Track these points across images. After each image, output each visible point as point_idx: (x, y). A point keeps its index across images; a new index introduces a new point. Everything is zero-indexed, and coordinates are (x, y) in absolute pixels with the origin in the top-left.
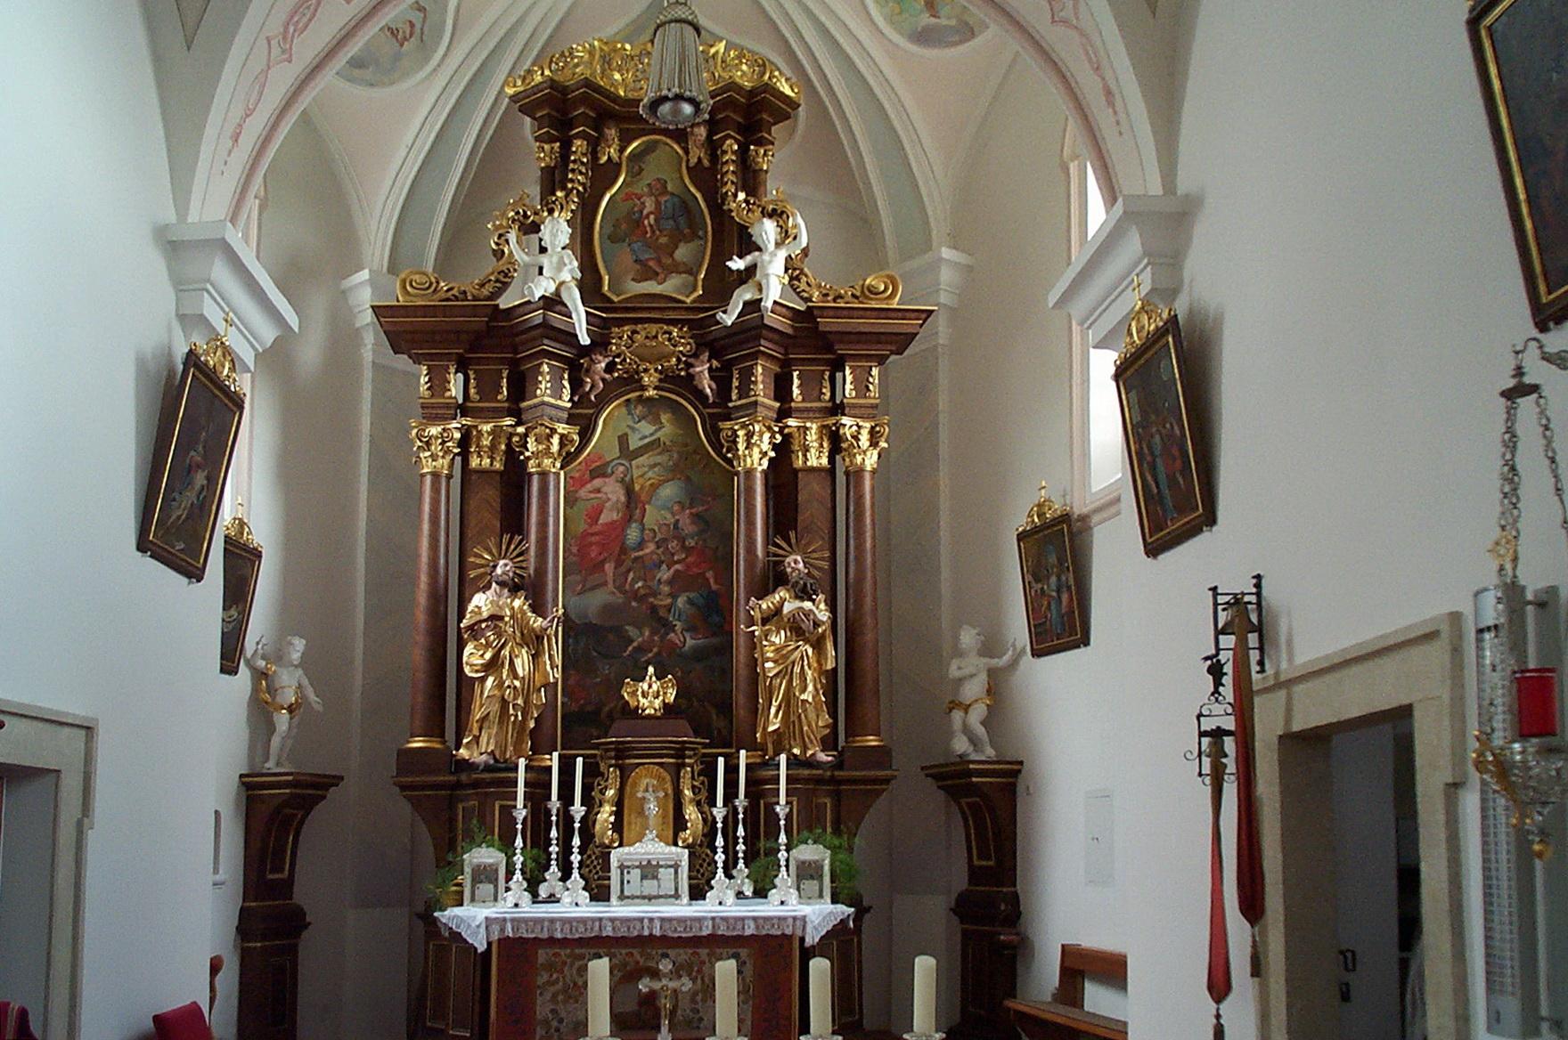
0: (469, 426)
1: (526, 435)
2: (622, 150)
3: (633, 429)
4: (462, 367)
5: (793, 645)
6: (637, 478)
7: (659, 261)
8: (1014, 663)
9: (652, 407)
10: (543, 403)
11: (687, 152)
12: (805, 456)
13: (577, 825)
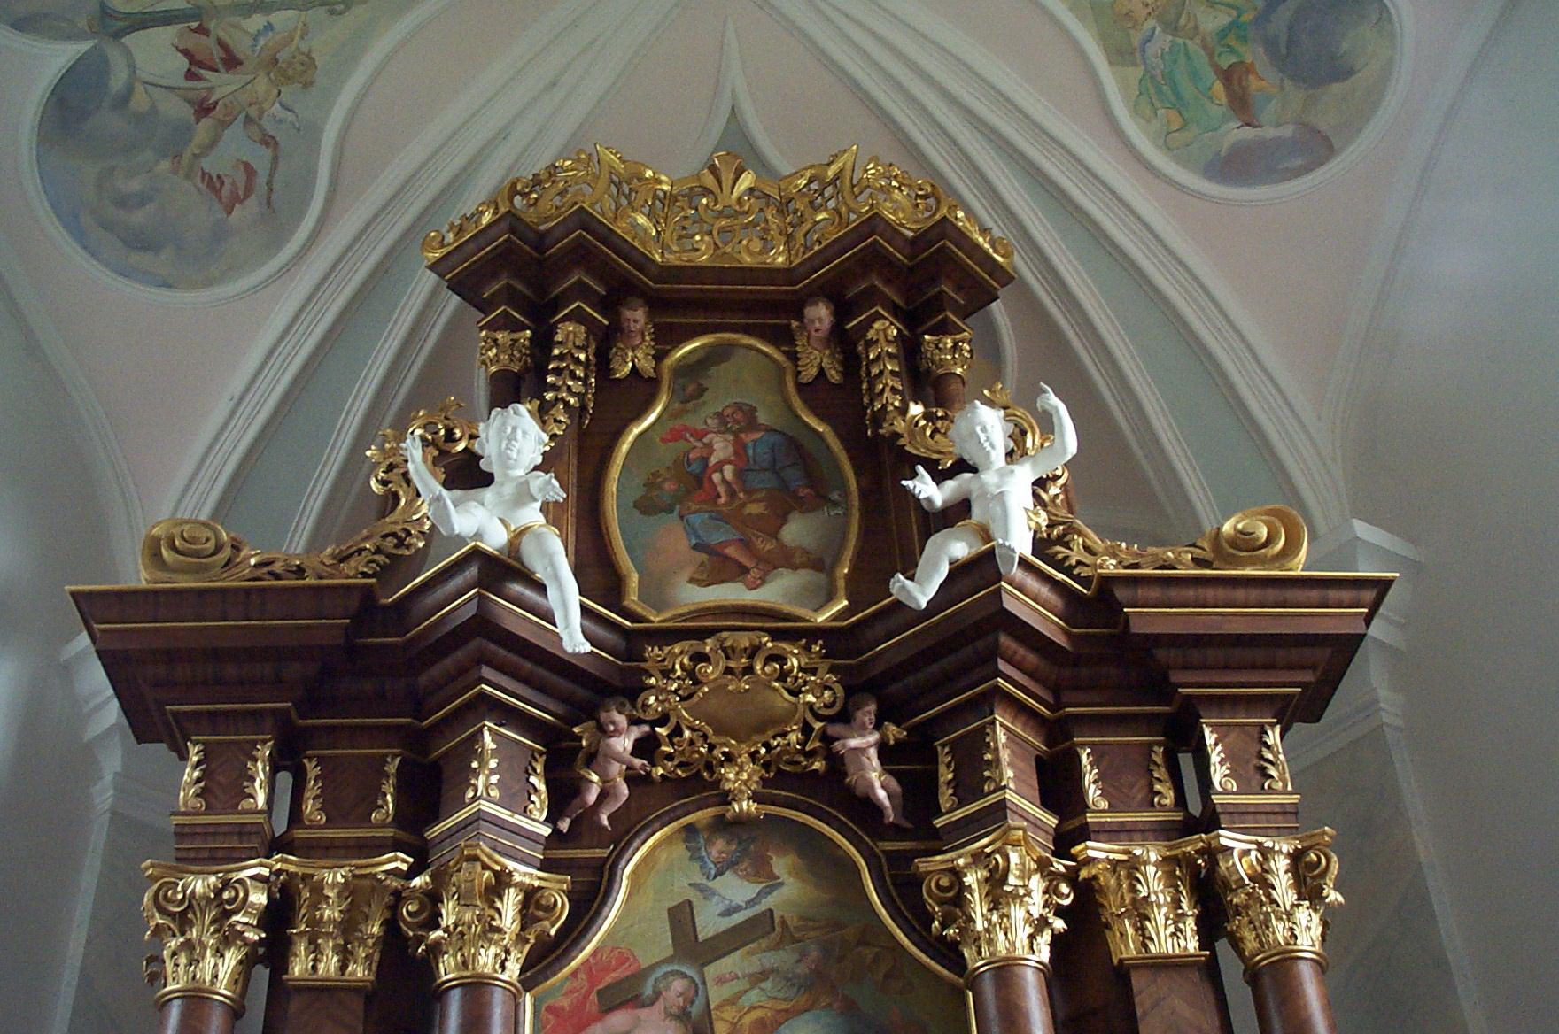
0: (291, 875)
2: (659, 357)
3: (702, 889)
4: (287, 759)
6: (719, 1007)
7: (746, 544)
11: (793, 357)
12: (1141, 930)
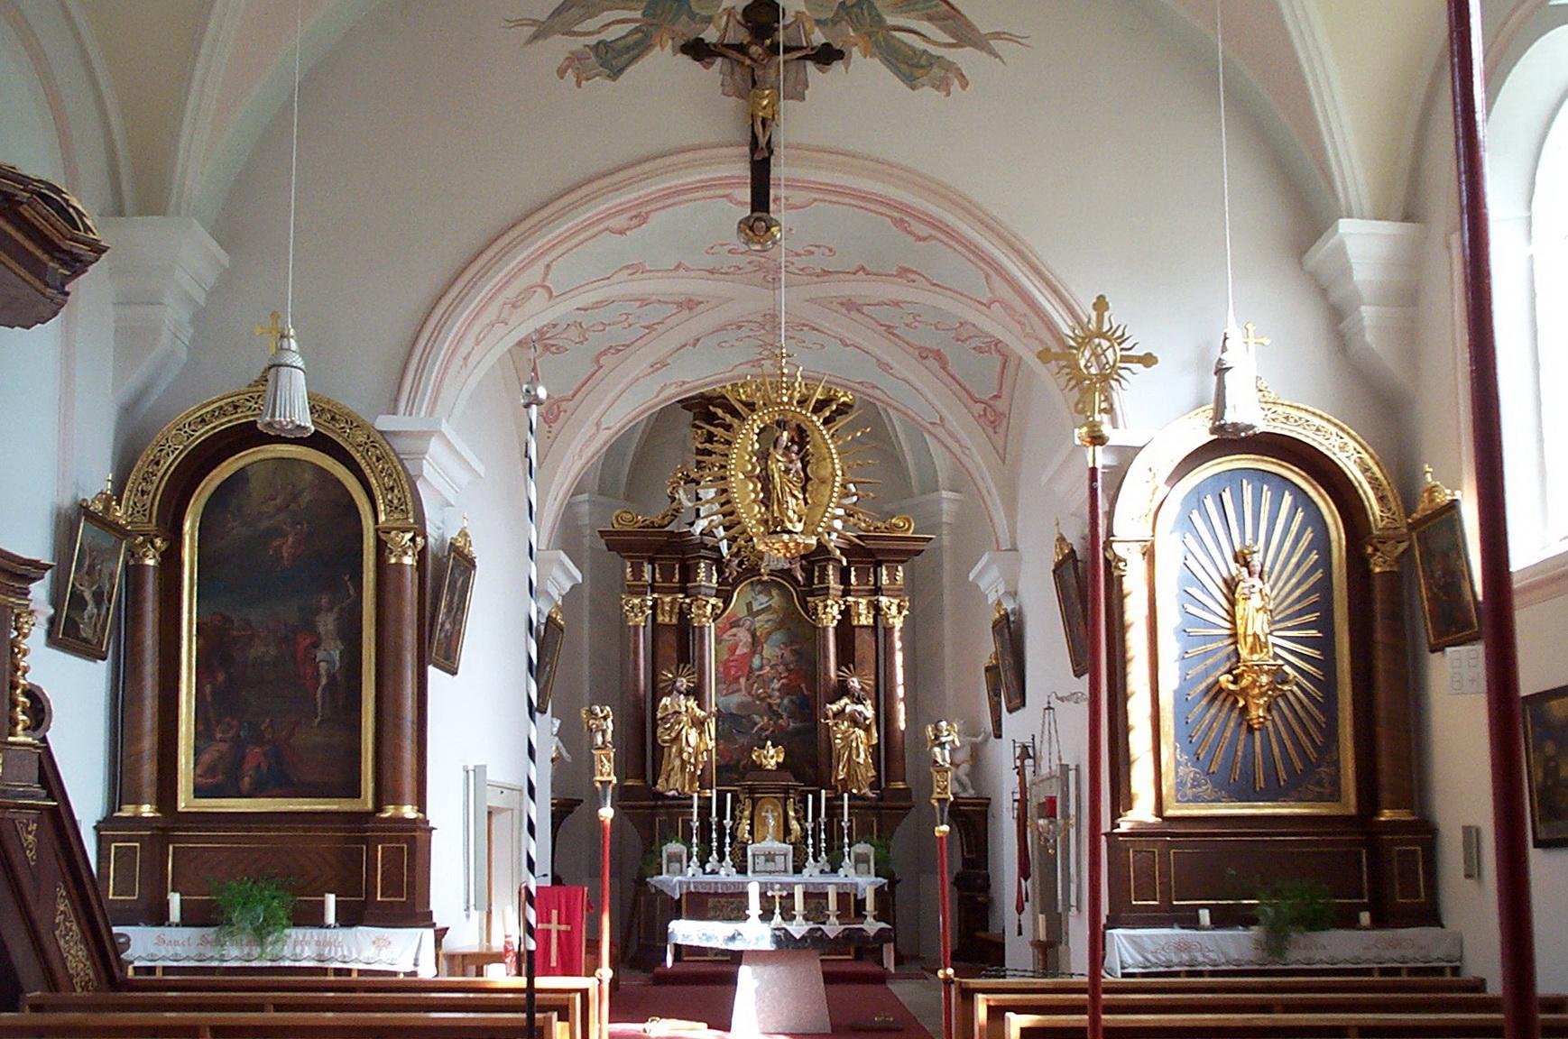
1: (692, 603)
4: (651, 562)
5: (851, 730)
8: (986, 740)
9: (766, 587)
10: (700, 586)
13: (728, 831)
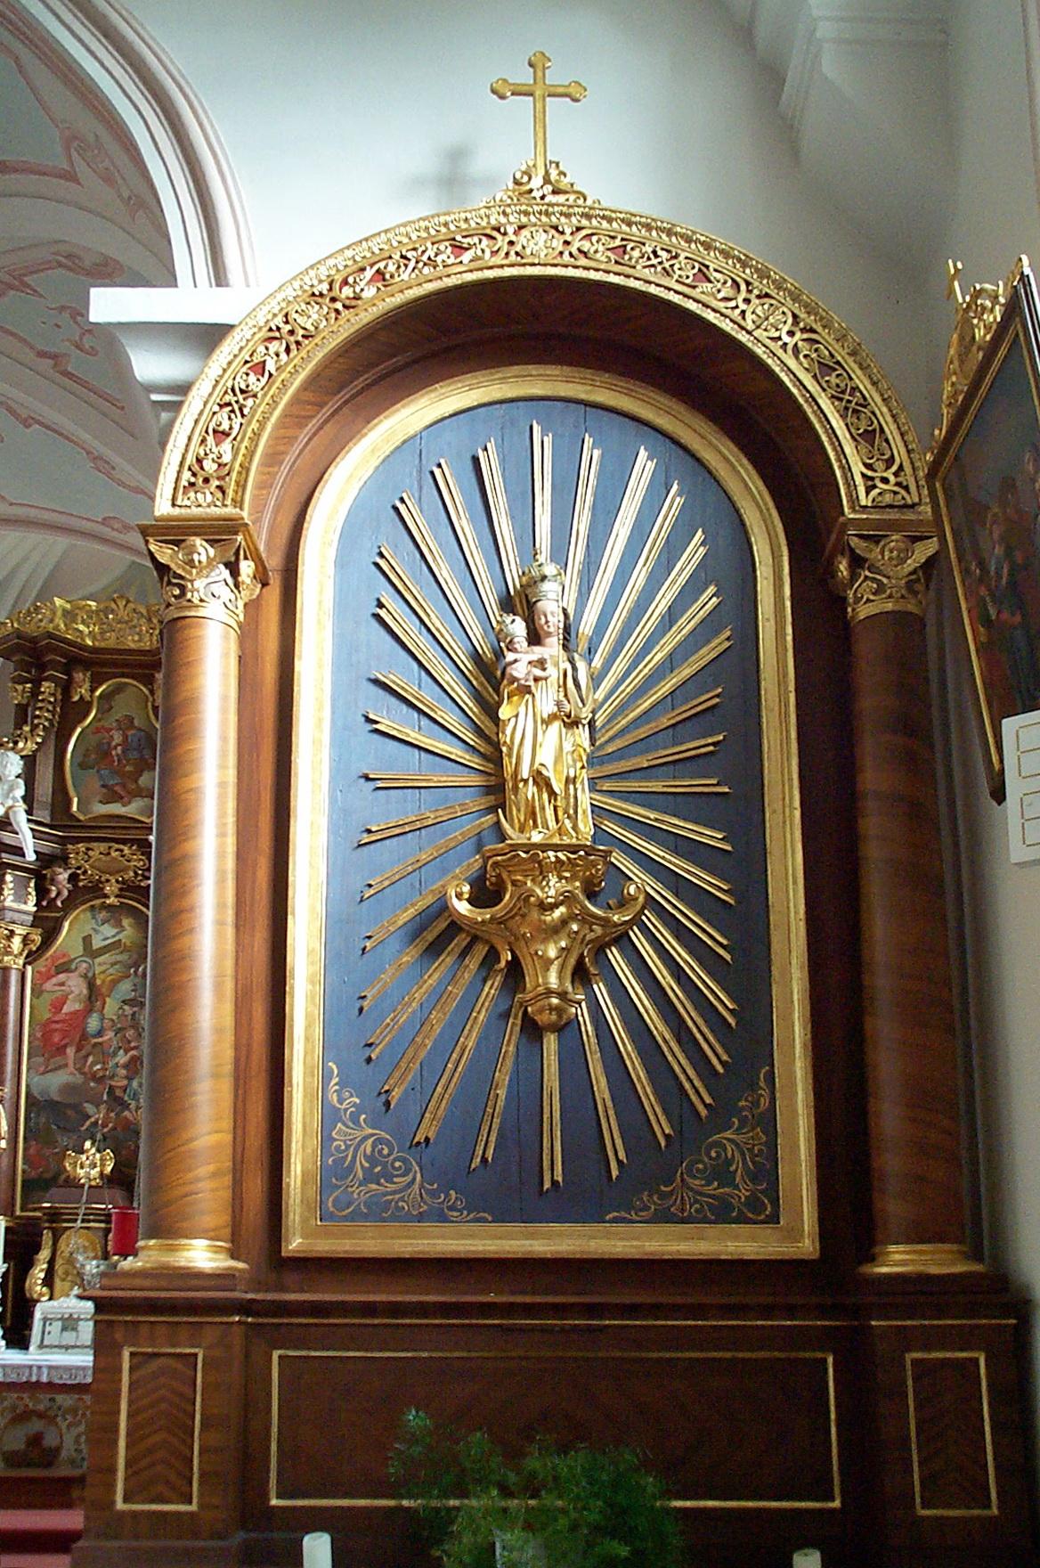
2: (93, 690)
7: (124, 786)
11: (152, 692)
